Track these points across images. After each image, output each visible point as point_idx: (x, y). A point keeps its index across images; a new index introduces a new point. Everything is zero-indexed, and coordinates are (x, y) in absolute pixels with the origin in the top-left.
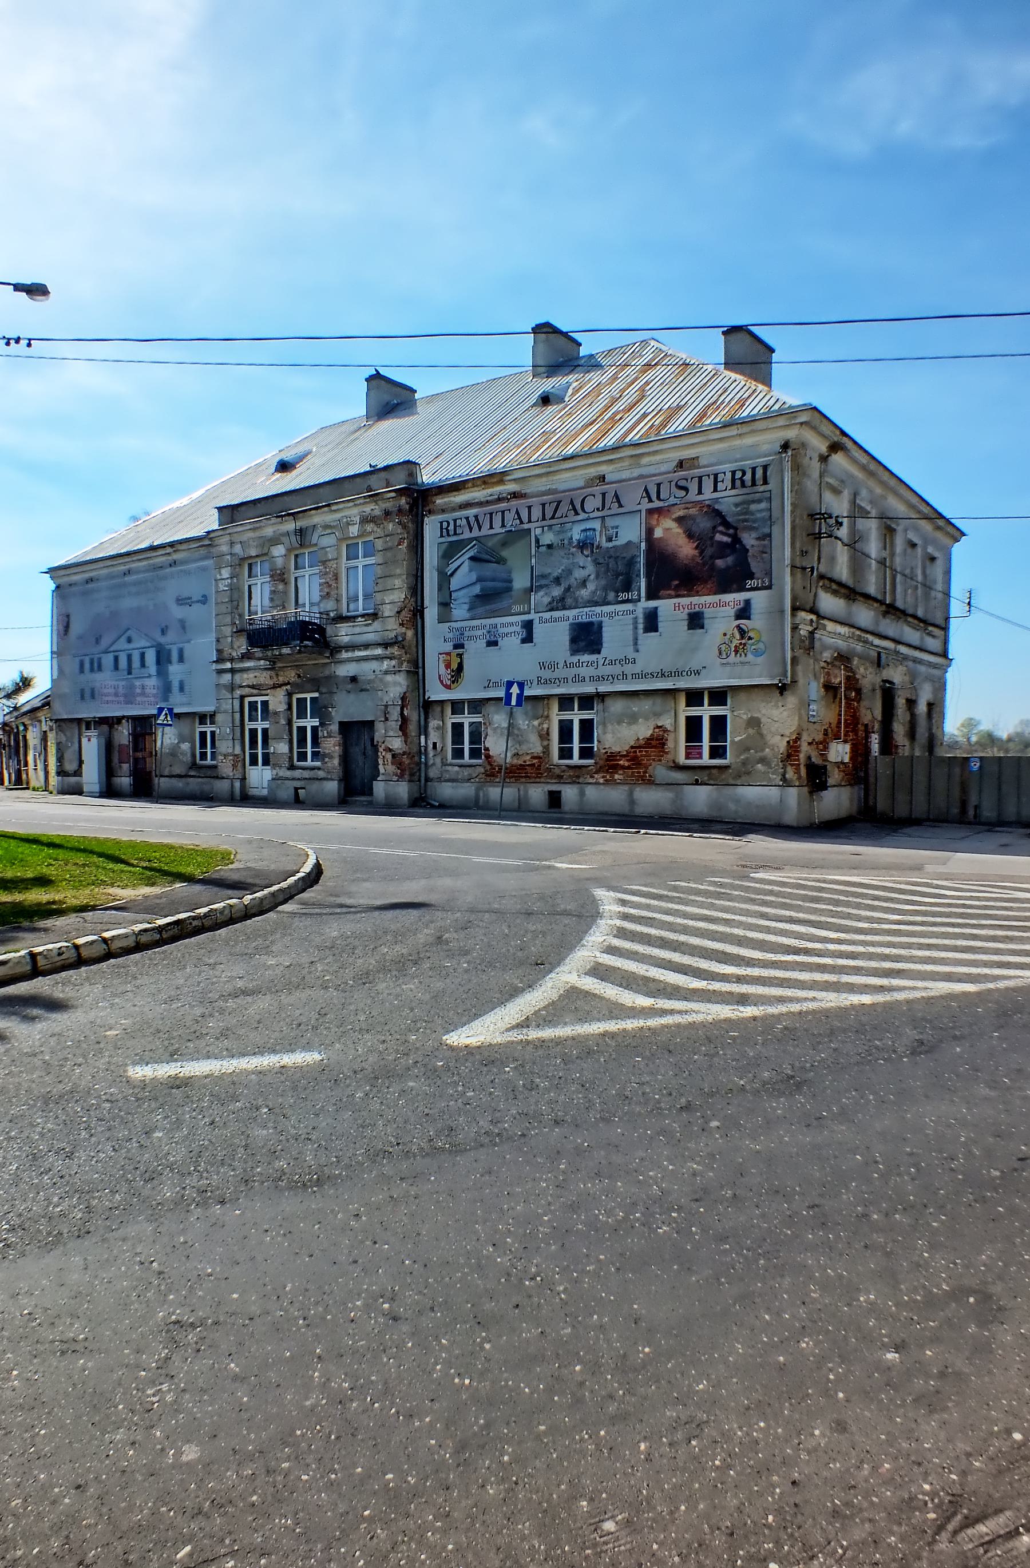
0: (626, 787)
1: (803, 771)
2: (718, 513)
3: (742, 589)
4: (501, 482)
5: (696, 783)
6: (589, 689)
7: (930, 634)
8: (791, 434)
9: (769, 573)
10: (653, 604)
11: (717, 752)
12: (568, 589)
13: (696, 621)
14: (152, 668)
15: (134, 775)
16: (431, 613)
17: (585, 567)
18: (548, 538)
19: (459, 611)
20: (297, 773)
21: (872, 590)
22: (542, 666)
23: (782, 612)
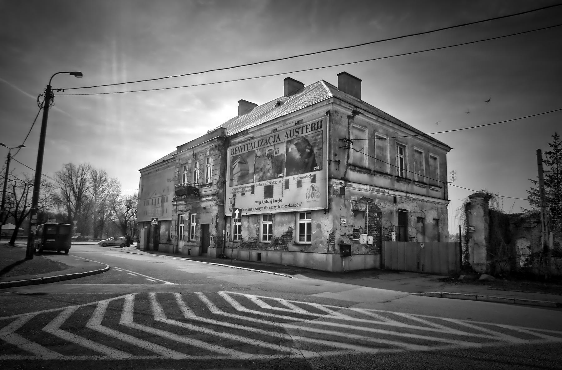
0: (280, 253)
1: (337, 247)
2: (307, 141)
3: (312, 170)
4: (248, 134)
5: (301, 251)
6: (268, 212)
7: (433, 189)
8: (330, 108)
9: (321, 163)
10: (288, 178)
11: (309, 239)
12: (264, 173)
13: (299, 184)
14: (160, 204)
15: (154, 245)
16: (228, 183)
17: (269, 164)
18: (259, 153)
19: (235, 182)
20: (190, 244)
21: (388, 170)
22: (256, 203)
23: (326, 179)
